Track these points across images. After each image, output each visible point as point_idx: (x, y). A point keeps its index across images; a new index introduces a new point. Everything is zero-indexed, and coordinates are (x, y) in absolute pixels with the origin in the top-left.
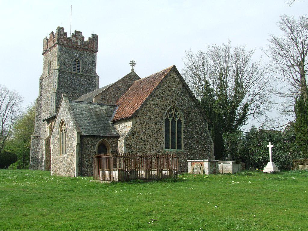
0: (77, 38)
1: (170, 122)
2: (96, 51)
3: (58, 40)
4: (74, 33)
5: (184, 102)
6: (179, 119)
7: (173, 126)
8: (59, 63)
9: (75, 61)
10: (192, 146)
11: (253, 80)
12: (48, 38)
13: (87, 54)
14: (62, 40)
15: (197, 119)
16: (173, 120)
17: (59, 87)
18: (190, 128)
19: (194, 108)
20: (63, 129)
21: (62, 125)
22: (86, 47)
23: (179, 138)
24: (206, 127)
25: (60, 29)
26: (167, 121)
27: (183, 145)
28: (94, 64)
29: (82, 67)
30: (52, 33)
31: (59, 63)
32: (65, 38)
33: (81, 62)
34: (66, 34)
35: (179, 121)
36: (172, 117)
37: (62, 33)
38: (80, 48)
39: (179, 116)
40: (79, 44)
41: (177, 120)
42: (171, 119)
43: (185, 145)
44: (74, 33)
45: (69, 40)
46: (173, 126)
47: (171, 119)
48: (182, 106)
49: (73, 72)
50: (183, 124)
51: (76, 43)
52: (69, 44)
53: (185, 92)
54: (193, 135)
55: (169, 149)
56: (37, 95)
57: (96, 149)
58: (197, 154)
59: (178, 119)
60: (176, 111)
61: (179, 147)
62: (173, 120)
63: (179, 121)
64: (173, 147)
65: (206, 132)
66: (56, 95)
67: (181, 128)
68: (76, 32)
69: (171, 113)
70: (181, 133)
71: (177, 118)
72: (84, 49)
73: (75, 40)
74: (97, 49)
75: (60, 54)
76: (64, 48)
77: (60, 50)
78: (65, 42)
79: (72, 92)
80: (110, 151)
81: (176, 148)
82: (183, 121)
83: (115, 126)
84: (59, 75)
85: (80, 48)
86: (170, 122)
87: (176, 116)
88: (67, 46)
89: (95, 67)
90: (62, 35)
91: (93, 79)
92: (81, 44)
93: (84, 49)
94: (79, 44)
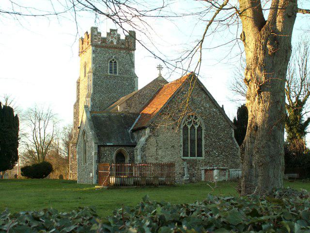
0: (112, 38)
1: (196, 130)
2: (134, 50)
3: (92, 42)
4: (109, 32)
5: (205, 108)
6: (199, 126)
7: (192, 134)
8: (93, 65)
9: (111, 62)
10: (215, 154)
11: (243, 91)
12: (83, 37)
13: (124, 53)
14: (96, 41)
15: (220, 125)
16: (193, 127)
17: (94, 91)
18: (212, 135)
19: (217, 114)
20: (85, 138)
21: (84, 135)
22: (123, 46)
23: (200, 146)
24: (231, 133)
25: (94, 29)
26: (185, 128)
27: (203, 153)
28: (132, 64)
29: (119, 68)
30: (87, 33)
31: (93, 65)
32: (99, 38)
33: (117, 63)
34: (100, 33)
35: (200, 129)
36: (191, 125)
37: (96, 33)
38: (116, 48)
39: (199, 124)
40: (115, 43)
41: (196, 127)
42: (189, 127)
43: (206, 152)
44: (109, 32)
45: (104, 40)
46: (192, 134)
47: (189, 127)
48: (202, 113)
49: (109, 74)
50: (203, 131)
51: (112, 42)
52: (104, 44)
53: (205, 98)
54: (215, 142)
55: (188, 156)
56: (75, 100)
57: (114, 158)
58: (221, 162)
59: (198, 126)
60: (196, 118)
61: (200, 155)
62: (193, 127)
63: (200, 129)
64: (193, 155)
65: (232, 138)
66: (92, 101)
67: (202, 135)
68: (111, 30)
69: (190, 120)
70: (201, 140)
71: (197, 125)
72: (121, 48)
73: (111, 39)
74: (135, 47)
75: (94, 55)
76: (99, 49)
77: (94, 52)
78: (100, 43)
79: (108, 96)
80: (127, 160)
81: (196, 155)
82: (204, 128)
83: (134, 133)
84: (94, 79)
85: (116, 48)
86: (196, 130)
87: (196, 124)
88: (103, 47)
89: (133, 67)
90: (96, 36)
91: (132, 79)
92: (117, 43)
93: (121, 48)
94: (115, 43)
